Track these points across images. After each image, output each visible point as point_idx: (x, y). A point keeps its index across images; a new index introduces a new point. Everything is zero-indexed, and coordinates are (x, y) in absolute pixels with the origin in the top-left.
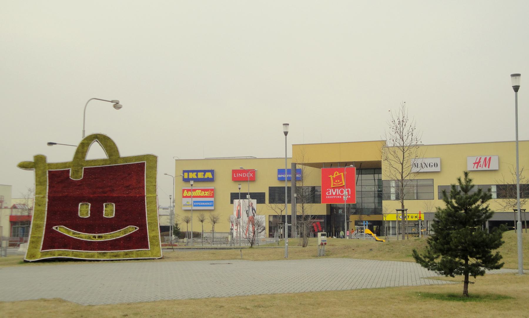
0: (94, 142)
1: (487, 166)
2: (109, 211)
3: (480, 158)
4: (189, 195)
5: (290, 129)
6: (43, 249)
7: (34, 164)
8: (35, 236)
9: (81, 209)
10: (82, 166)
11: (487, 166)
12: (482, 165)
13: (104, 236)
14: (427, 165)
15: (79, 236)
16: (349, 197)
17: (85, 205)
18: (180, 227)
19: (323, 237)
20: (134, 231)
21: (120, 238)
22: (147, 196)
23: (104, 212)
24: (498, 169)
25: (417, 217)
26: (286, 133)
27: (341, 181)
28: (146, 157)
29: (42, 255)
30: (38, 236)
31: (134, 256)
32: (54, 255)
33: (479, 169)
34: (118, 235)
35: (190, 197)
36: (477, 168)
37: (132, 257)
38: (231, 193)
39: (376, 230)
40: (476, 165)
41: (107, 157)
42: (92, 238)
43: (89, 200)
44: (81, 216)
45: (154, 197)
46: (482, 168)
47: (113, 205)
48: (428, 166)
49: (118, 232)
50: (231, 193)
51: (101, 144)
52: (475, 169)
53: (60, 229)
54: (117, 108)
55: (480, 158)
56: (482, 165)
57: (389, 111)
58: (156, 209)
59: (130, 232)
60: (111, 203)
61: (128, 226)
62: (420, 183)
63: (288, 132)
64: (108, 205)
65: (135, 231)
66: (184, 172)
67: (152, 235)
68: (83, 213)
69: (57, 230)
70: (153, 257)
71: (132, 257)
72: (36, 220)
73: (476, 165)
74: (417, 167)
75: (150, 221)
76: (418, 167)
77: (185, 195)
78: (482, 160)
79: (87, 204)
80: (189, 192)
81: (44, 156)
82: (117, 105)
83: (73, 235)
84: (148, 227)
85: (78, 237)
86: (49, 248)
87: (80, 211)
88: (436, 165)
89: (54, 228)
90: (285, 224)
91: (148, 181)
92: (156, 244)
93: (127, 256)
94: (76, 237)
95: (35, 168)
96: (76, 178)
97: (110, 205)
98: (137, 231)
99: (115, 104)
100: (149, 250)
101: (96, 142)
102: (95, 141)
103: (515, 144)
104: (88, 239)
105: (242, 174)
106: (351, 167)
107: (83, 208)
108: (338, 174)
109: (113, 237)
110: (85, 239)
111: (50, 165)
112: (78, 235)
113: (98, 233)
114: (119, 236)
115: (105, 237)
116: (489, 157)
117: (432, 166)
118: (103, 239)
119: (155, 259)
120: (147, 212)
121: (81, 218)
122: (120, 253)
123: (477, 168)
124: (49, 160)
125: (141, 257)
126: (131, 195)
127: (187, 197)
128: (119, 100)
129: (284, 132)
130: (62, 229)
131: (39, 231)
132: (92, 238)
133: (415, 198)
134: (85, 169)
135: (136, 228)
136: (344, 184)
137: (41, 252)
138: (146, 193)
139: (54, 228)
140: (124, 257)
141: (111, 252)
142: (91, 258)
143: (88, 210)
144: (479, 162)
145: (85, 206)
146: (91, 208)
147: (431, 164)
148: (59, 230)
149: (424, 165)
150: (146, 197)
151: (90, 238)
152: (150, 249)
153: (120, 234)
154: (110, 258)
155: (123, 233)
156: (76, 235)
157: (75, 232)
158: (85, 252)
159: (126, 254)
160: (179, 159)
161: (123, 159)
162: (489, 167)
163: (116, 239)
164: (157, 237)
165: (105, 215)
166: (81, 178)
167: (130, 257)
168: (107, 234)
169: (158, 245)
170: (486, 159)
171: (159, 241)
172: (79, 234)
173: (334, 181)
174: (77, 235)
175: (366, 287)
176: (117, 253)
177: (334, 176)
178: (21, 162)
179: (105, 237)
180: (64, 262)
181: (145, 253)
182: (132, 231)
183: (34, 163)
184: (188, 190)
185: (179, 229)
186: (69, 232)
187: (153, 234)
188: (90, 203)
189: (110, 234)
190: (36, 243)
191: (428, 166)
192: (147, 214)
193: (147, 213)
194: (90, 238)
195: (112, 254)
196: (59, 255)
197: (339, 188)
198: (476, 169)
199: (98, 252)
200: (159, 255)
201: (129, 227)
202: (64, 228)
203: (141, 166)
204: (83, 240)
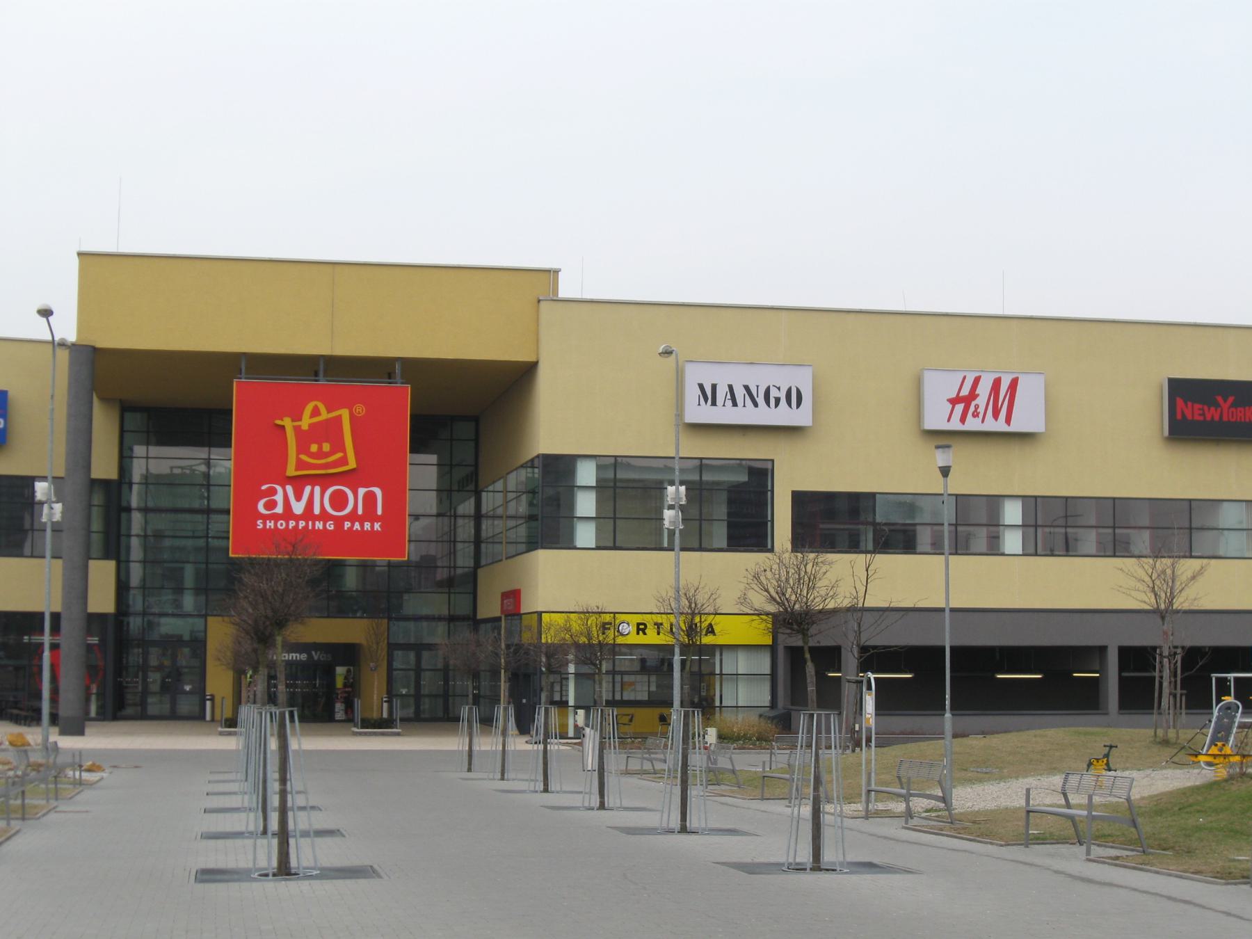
12: (981, 410)
16: (372, 527)
27: (339, 446)
33: (972, 424)
36: (963, 420)
38: (793, 492)
39: (345, 685)
40: (960, 408)
46: (983, 421)
48: (761, 400)
50: (793, 492)
52: (955, 425)
56: (981, 410)
73: (960, 408)
74: (709, 401)
76: (714, 403)
78: (984, 390)
88: (794, 398)
108: (325, 415)
117: (778, 401)
123: (963, 420)
133: (666, 545)
136: (352, 464)
144: (973, 395)
147: (774, 393)
149: (740, 393)
162: (1008, 421)
170: (997, 383)
173: (302, 448)
177: (305, 423)
191: (761, 400)
197: (324, 481)
198: (959, 427)
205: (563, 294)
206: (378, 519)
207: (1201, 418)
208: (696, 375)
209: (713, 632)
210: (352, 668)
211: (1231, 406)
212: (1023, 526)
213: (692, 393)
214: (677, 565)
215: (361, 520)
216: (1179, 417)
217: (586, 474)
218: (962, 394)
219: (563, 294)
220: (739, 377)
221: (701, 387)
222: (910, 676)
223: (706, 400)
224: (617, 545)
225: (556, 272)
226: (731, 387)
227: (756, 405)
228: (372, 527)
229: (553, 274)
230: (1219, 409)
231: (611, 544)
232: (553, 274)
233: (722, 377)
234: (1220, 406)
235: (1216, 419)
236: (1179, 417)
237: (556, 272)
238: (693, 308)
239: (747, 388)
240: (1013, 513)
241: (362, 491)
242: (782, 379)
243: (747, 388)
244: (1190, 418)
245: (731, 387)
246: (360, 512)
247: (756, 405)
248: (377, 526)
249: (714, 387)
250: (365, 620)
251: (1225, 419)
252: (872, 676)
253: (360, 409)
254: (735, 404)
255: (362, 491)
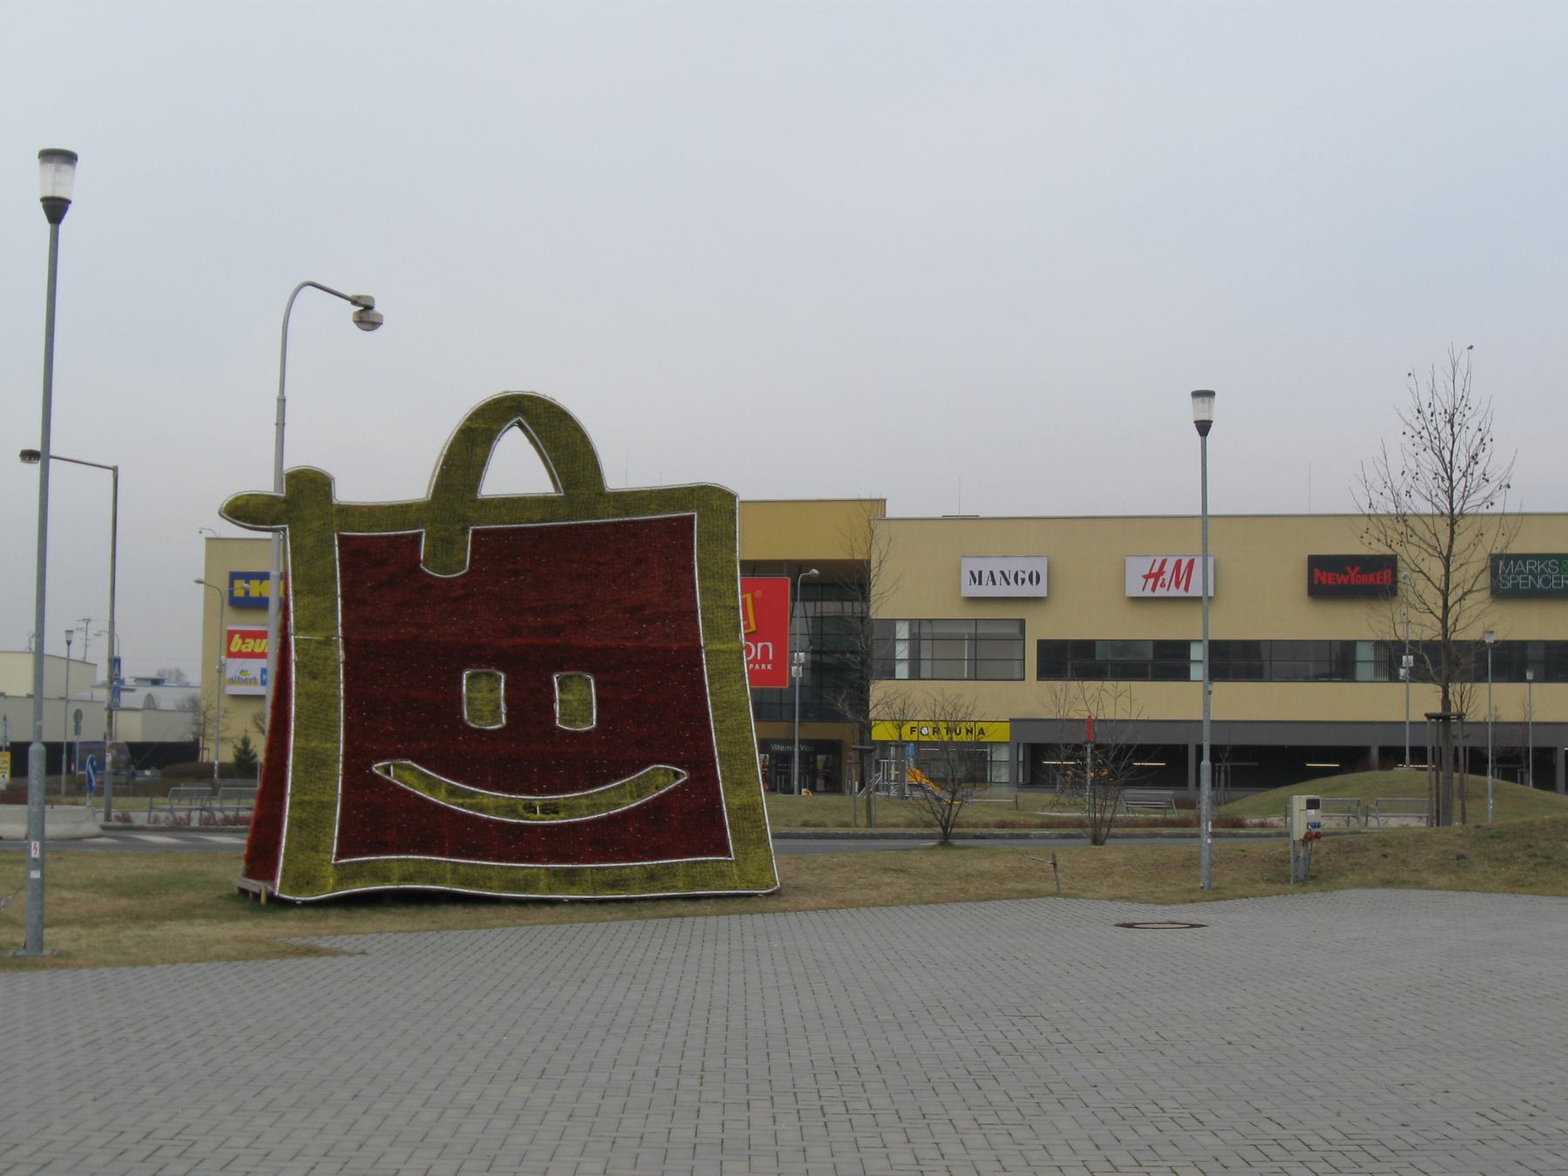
0: (511, 427)
1: (1183, 584)
2: (575, 704)
3: (1164, 563)
4: (249, 650)
5: (1218, 412)
6: (340, 855)
7: (284, 506)
8: (307, 798)
9: (472, 695)
10: (466, 522)
11: (1183, 584)
12: (1167, 583)
13: (564, 805)
14: (1003, 579)
15: (474, 801)
16: (766, 667)
17: (484, 678)
18: (255, 750)
19: (1312, 812)
20: (673, 785)
21: (623, 813)
22: (709, 647)
23: (557, 707)
24: (1045, 595)
25: (972, 733)
26: (1204, 427)
28: (695, 495)
29: (341, 878)
30: (322, 802)
31: (681, 885)
32: (386, 879)
33: (1160, 592)
34: (615, 800)
35: (252, 655)
36: (1153, 589)
37: (673, 887)
38: (1038, 641)
39: (825, 767)
40: (1151, 581)
41: (553, 491)
42: (521, 810)
43: (500, 659)
44: (473, 722)
45: (731, 652)
46: (1168, 590)
47: (588, 681)
48: (1012, 580)
49: (613, 788)
50: (1038, 641)
51: (537, 439)
52: (1148, 593)
53: (401, 772)
54: (367, 326)
55: (1164, 563)
56: (1167, 583)
57: (1410, 375)
58: (743, 698)
59: (657, 788)
60: (580, 673)
61: (647, 766)
62: (982, 630)
63: (1212, 422)
64: (567, 681)
65: (676, 787)
66: (234, 576)
67: (736, 801)
68: (480, 710)
69: (387, 777)
70: (749, 888)
71: (673, 887)
72: (307, 735)
73: (1151, 581)
74: (977, 582)
75: (725, 749)
76: (980, 583)
77: (234, 649)
78: (1169, 568)
79: (491, 675)
80: (247, 640)
81: (322, 474)
82: (367, 316)
83: (451, 800)
84: (722, 772)
85: (470, 809)
86: (364, 850)
87: (469, 704)
88: (1034, 578)
89: (377, 768)
90: (1203, 763)
91: (707, 588)
92: (754, 836)
93: (655, 883)
94: (462, 805)
95: (290, 521)
96: (444, 570)
97: (575, 679)
98: (682, 784)
99: (361, 311)
100: (731, 862)
101: (516, 430)
102: (513, 425)
103: (1199, 522)
104: (506, 815)
105: (1324, 573)
106: (813, 574)
107: (479, 692)
109: (595, 807)
110: (497, 814)
111: (347, 511)
112: (468, 801)
113: (542, 792)
114: (619, 805)
115: (571, 809)
116: (1177, 558)
117: (1023, 581)
118: (562, 815)
119: (756, 895)
120: (713, 712)
121: (473, 729)
122: (628, 871)
123: (1153, 589)
124: (343, 494)
125: (705, 886)
126: (652, 645)
127: (240, 655)
128: (374, 296)
129: (1195, 422)
130: (407, 775)
131: (320, 779)
132: (521, 810)
133: (966, 676)
134: (475, 533)
135: (677, 776)
137: (335, 865)
138: (705, 639)
139: (376, 768)
140: (643, 890)
141: (597, 869)
142: (524, 890)
143: (498, 699)
144: (1161, 572)
145: (484, 683)
146: (506, 691)
147: (1021, 575)
148: (396, 777)
149: (998, 576)
150: (706, 653)
151: (512, 811)
152: (733, 858)
153: (624, 797)
154: (595, 894)
155: (635, 795)
156: (460, 801)
157: (458, 787)
158: (501, 867)
159: (651, 877)
160: (218, 536)
161: (617, 501)
162: (1186, 589)
163: (610, 817)
164: (754, 809)
165: (560, 719)
166: (464, 569)
167: (663, 889)
168: (575, 798)
169: (762, 840)
170: (1178, 564)
171: (765, 824)
172: (472, 794)
174: (463, 798)
175: (646, 922)
176: (617, 872)
178: (237, 498)
179: (571, 809)
180: (426, 907)
181: (721, 875)
182: (666, 785)
183: (285, 501)
184: (245, 635)
185: (252, 754)
186: (432, 786)
187: (741, 798)
188: (504, 671)
189: (587, 796)
190: (313, 827)
191: (1012, 580)
192: (715, 721)
193: (714, 716)
194: (512, 811)
195: (599, 877)
196: (404, 879)
198: (1152, 595)
199: (547, 869)
200: (767, 880)
201: (653, 770)
202: (414, 769)
203: (683, 528)
204: (489, 821)
205: (888, 515)
206: (770, 662)
207: (1334, 583)
208: (970, 565)
209: (983, 733)
210: (831, 756)
211: (1359, 573)
212: (1375, 662)
213: (966, 577)
214: (1408, 690)
215: (760, 663)
216: (1316, 582)
217: (903, 631)
218: (1153, 571)
219: (888, 515)
220: (997, 566)
221: (972, 573)
222: (1308, 765)
223: (975, 582)
224: (978, 677)
225: (885, 501)
226: (991, 573)
227: (1008, 583)
228: (766, 667)
229: (882, 502)
230: (1348, 576)
231: (973, 677)
232: (882, 502)
233: (985, 566)
234: (1348, 574)
235: (1346, 583)
236: (1316, 582)
237: (885, 501)
238: (914, 521)
239: (1002, 573)
240: (1197, 653)
241: (760, 645)
242: (1025, 566)
243: (1002, 573)
244: (1324, 582)
245: (991, 573)
246: (759, 658)
247: (1008, 583)
248: (769, 667)
249: (980, 573)
250: (785, 723)
251: (1352, 583)
252: (1228, 764)
253: (758, 593)
254: (994, 583)
255: (760, 645)
